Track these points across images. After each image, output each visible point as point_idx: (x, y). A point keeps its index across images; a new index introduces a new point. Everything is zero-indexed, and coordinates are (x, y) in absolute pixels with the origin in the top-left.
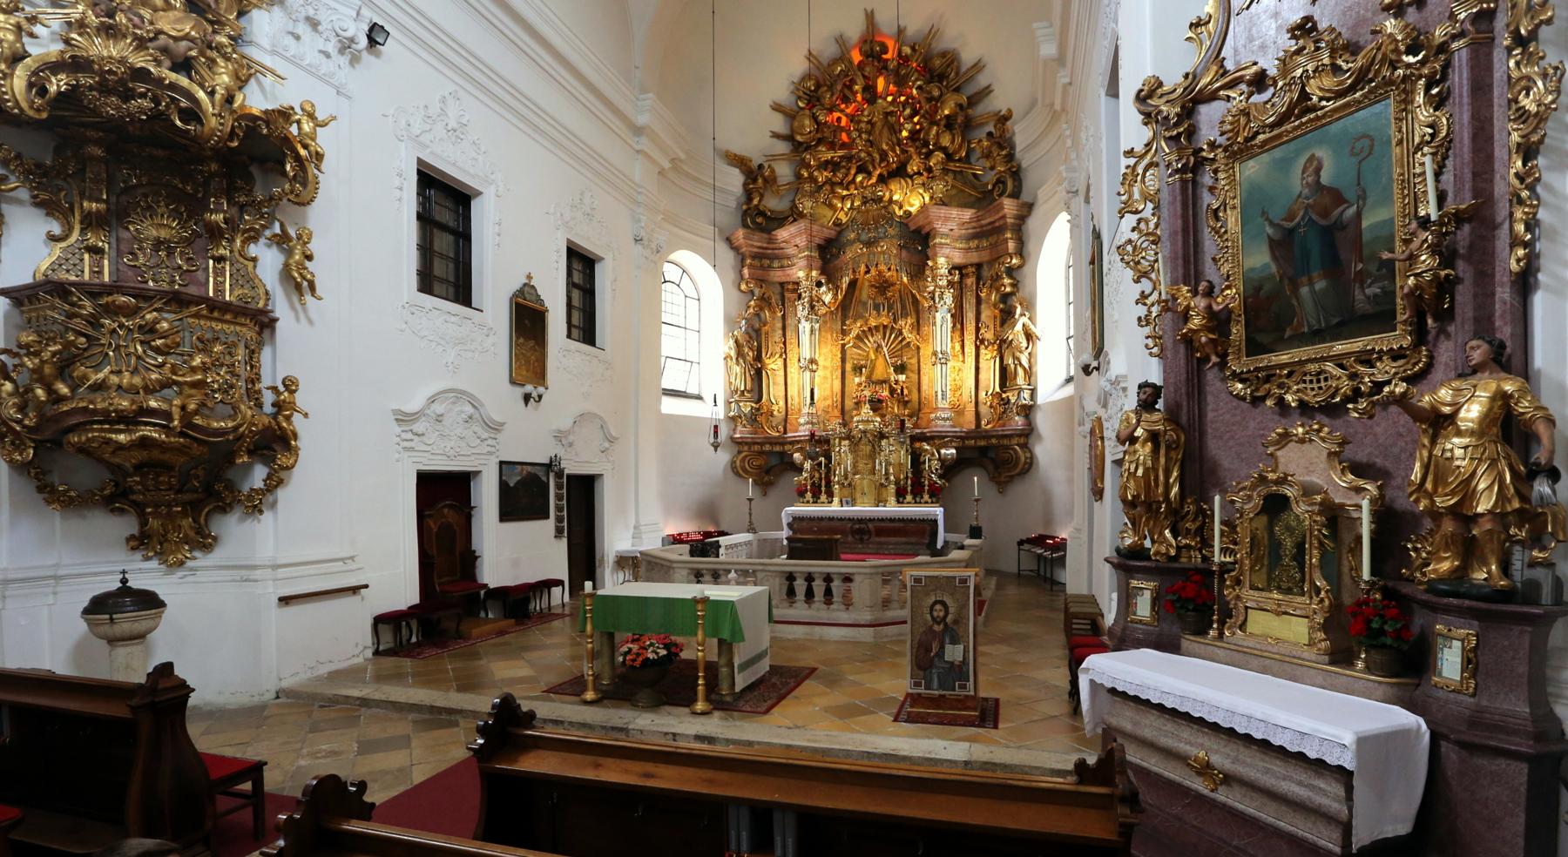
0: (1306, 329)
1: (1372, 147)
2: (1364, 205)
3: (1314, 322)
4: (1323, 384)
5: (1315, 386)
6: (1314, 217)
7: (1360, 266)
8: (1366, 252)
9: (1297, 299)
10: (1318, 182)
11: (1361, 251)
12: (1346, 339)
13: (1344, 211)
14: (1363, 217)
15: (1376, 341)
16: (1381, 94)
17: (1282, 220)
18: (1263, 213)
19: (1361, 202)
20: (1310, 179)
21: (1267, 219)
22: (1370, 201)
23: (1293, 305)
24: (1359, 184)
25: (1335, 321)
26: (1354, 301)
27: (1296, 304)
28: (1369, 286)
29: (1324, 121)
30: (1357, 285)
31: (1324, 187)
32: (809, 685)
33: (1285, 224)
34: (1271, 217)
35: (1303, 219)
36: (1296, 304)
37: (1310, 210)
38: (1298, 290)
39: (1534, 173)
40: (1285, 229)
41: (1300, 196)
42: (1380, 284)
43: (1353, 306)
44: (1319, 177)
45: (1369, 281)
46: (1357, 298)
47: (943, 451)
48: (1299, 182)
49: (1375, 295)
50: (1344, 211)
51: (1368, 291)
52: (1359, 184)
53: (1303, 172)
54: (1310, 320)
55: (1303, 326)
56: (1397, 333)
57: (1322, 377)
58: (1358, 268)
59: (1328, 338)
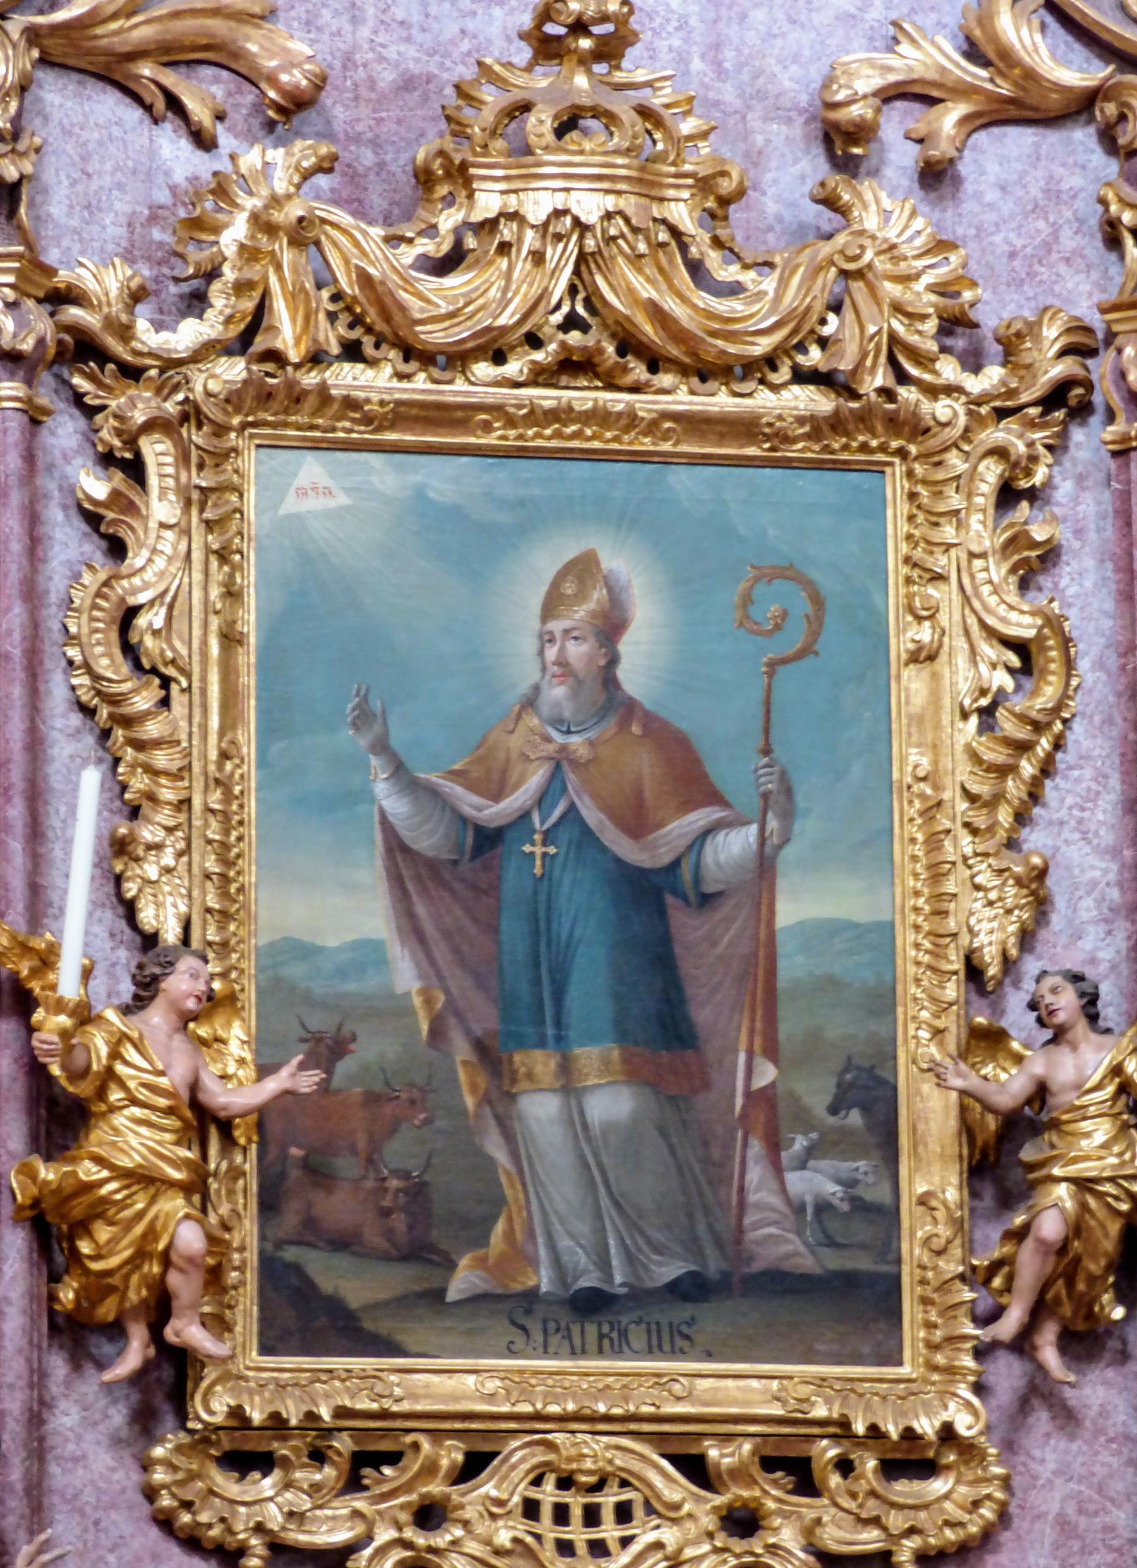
0: (544, 1280)
1: (816, 623)
2: (786, 840)
3: (580, 1259)
4: (609, 1531)
5: (578, 1534)
6: (592, 815)
7: (767, 1074)
8: (789, 1027)
9: (509, 1137)
10: (608, 678)
11: (771, 1018)
12: (709, 1356)
13: (708, 832)
14: (782, 884)
15: (848, 1388)
16: (864, 448)
17: (457, 776)
18: (363, 717)
19: (773, 823)
20: (577, 652)
21: (382, 747)
22: (806, 828)
23: (490, 1163)
24: (767, 751)
25: (668, 1271)
26: (742, 1205)
27: (500, 1154)
28: (802, 1165)
29: (646, 444)
30: (756, 1148)
31: (630, 708)
32: (143, 611)
33: (470, 803)
34: (397, 740)
35: (543, 800)
36: (500, 1154)
37: (572, 778)
38: (512, 1097)
39: (284, 1156)
40: (464, 820)
41: (530, 702)
42: (845, 1167)
43: (740, 1229)
44: (613, 660)
45: (800, 1143)
46: (752, 1198)
47: (9, 1379)
48: (530, 645)
49: (823, 1208)
50: (708, 832)
51: (798, 1182)
52: (767, 751)
53: (549, 611)
54: (564, 1242)
55: (534, 1262)
56: (906, 1370)
57: (608, 1500)
58: (759, 1082)
59: (637, 1336)
